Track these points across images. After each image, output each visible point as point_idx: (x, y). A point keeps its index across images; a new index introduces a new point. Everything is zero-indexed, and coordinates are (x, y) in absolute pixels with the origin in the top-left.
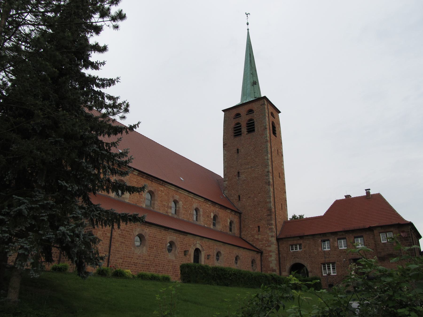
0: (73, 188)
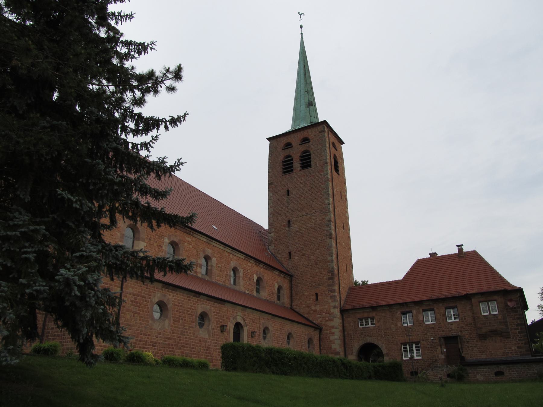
0: (81, 205)
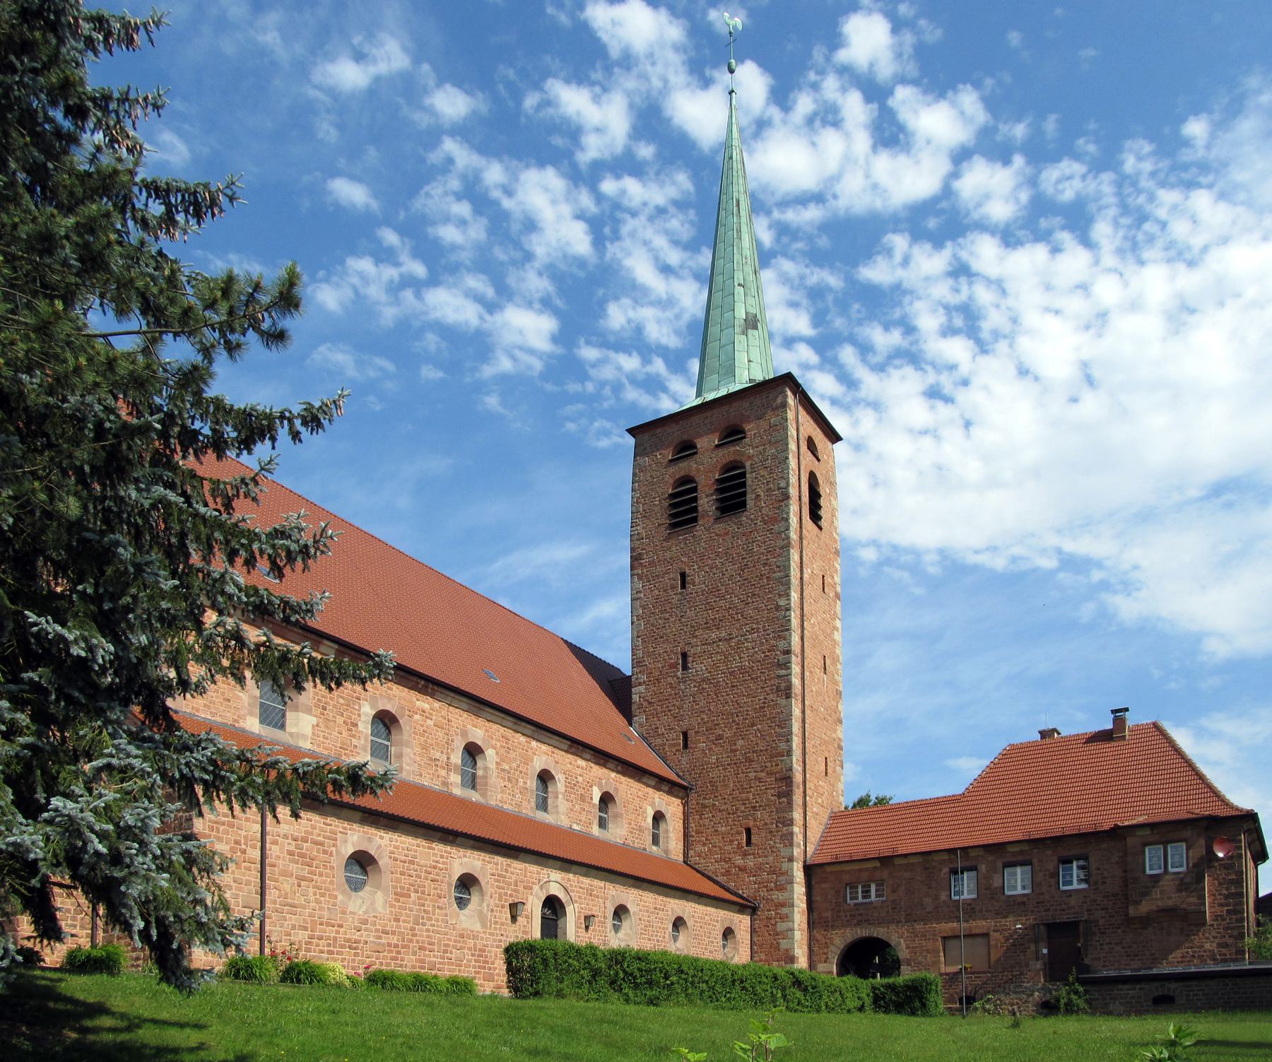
0: (91, 649)
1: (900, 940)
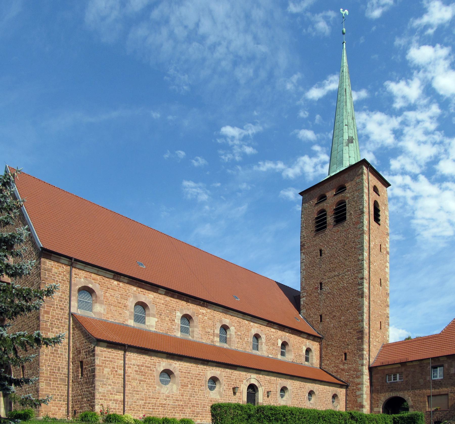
1: (408, 397)
